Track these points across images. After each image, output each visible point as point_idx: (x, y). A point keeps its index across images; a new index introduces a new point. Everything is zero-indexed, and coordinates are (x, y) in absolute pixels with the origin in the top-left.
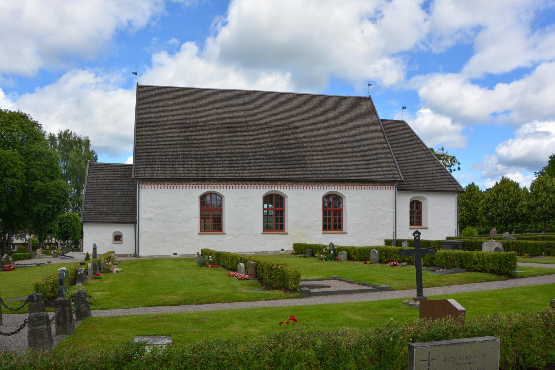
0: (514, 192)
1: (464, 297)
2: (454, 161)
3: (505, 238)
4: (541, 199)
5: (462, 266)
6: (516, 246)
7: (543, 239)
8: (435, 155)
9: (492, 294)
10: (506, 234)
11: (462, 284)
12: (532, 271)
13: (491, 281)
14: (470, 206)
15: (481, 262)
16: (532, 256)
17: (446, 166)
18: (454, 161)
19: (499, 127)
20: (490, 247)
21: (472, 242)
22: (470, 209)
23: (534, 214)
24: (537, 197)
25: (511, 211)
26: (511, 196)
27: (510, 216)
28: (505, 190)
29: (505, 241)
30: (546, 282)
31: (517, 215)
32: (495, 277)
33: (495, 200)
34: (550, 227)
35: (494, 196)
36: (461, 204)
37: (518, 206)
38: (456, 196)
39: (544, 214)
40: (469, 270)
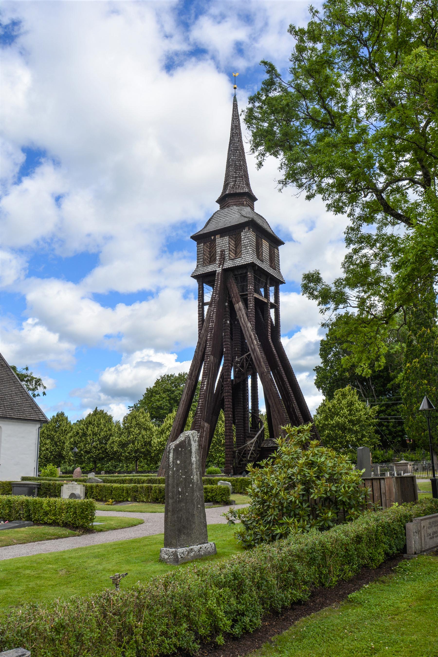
0: (105, 425)
1: (19, 565)
2: (40, 385)
3: (90, 480)
4: (133, 435)
5: (29, 518)
6: (101, 490)
7: (131, 481)
8: (18, 375)
9: (58, 559)
10: (91, 475)
11: (24, 543)
12: (112, 523)
13: (62, 538)
14: (56, 439)
15: (53, 512)
16: (118, 502)
17: (30, 389)
18: (40, 385)
19: (98, 353)
20: (72, 490)
21: (50, 485)
22: (56, 443)
23: (125, 451)
24: (129, 433)
25: (102, 448)
26: (102, 430)
27: (100, 453)
28: (95, 422)
29: (88, 484)
30: (127, 537)
31: (107, 453)
32: (68, 531)
33: (85, 434)
34: (142, 467)
35: (84, 430)
36: (42, 436)
37: (109, 442)
38: (38, 426)
39: (136, 452)
40: (38, 522)
